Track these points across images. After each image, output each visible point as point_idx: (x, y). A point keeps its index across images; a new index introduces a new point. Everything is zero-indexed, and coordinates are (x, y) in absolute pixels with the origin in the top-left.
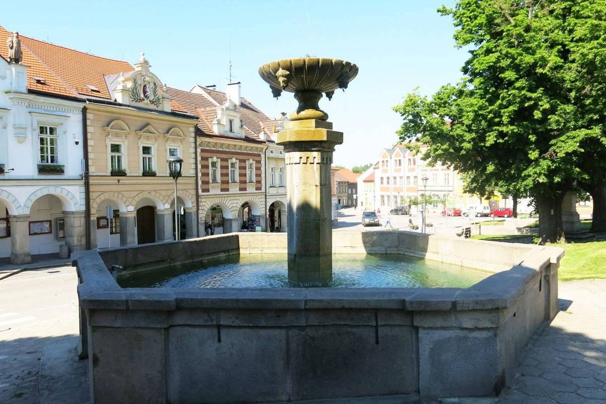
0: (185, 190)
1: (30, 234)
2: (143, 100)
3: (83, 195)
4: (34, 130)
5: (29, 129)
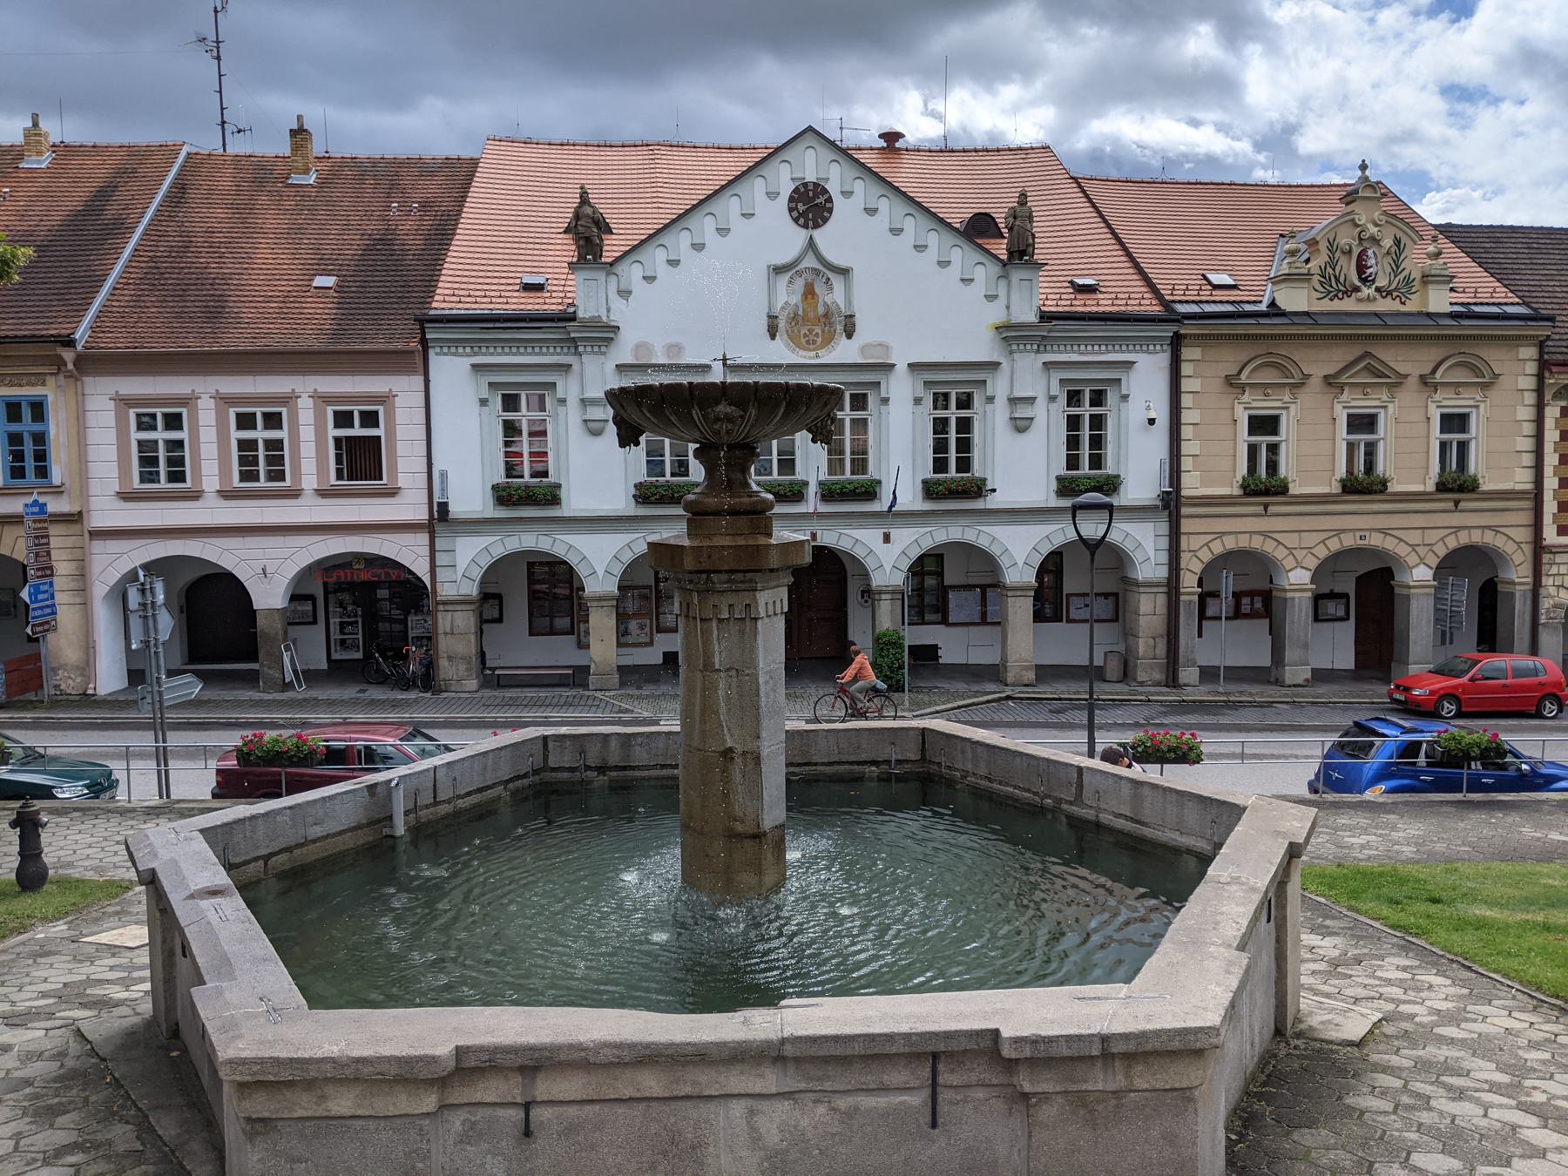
0: (1489, 527)
1: (1116, 620)
2: (1357, 289)
3: (1164, 543)
4: (1052, 399)
5: (1042, 401)
